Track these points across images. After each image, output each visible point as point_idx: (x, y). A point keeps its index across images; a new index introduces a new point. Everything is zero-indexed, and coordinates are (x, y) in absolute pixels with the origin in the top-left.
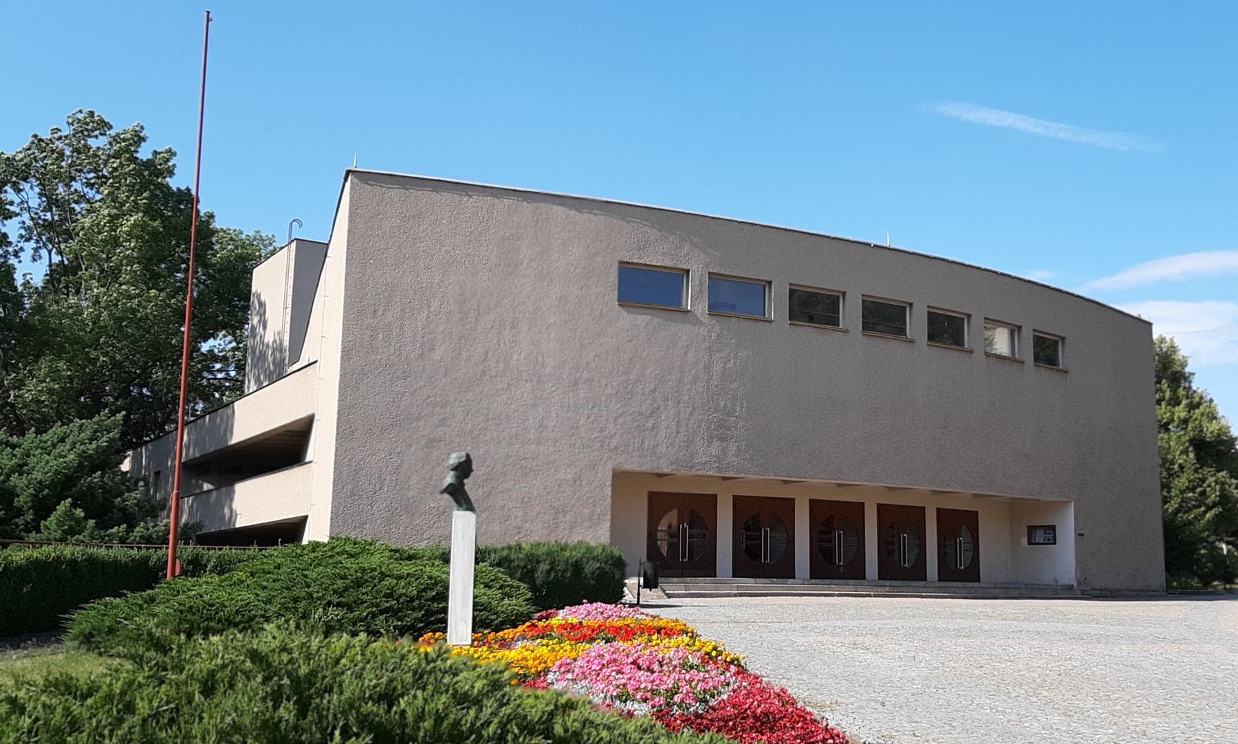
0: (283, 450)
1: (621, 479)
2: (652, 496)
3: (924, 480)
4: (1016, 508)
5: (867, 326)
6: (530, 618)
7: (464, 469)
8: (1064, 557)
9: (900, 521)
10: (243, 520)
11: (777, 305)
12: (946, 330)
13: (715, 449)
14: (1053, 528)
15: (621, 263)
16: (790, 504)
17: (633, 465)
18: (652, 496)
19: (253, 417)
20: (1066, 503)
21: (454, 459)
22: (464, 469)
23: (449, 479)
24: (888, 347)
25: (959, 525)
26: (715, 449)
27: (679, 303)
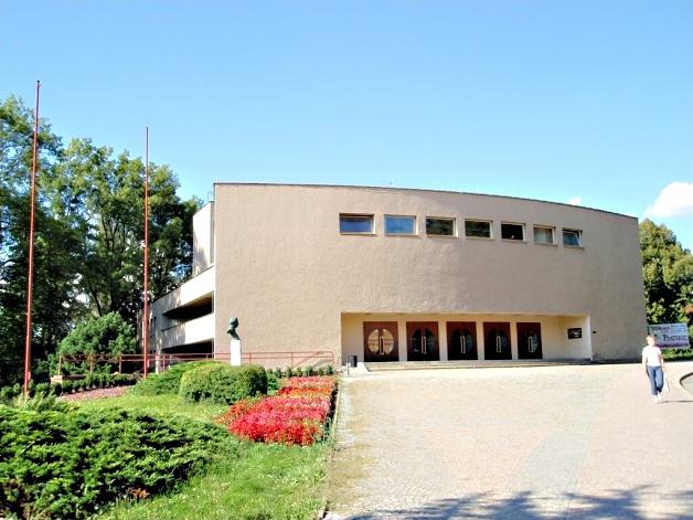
0: (202, 308)
1: (346, 317)
2: (365, 323)
3: (512, 312)
4: (561, 319)
5: (504, 236)
6: (140, 439)
7: (235, 324)
8: (586, 346)
9: (496, 331)
10: (189, 340)
11: (419, 228)
12: (571, 236)
13: (391, 301)
14: (579, 330)
15: (341, 215)
16: (435, 324)
17: (351, 310)
18: (365, 323)
19: (187, 294)
20: (582, 317)
21: (232, 320)
22: (235, 324)
23: (230, 327)
24: (479, 242)
25: (530, 331)
26: (391, 301)
27: (411, 232)
